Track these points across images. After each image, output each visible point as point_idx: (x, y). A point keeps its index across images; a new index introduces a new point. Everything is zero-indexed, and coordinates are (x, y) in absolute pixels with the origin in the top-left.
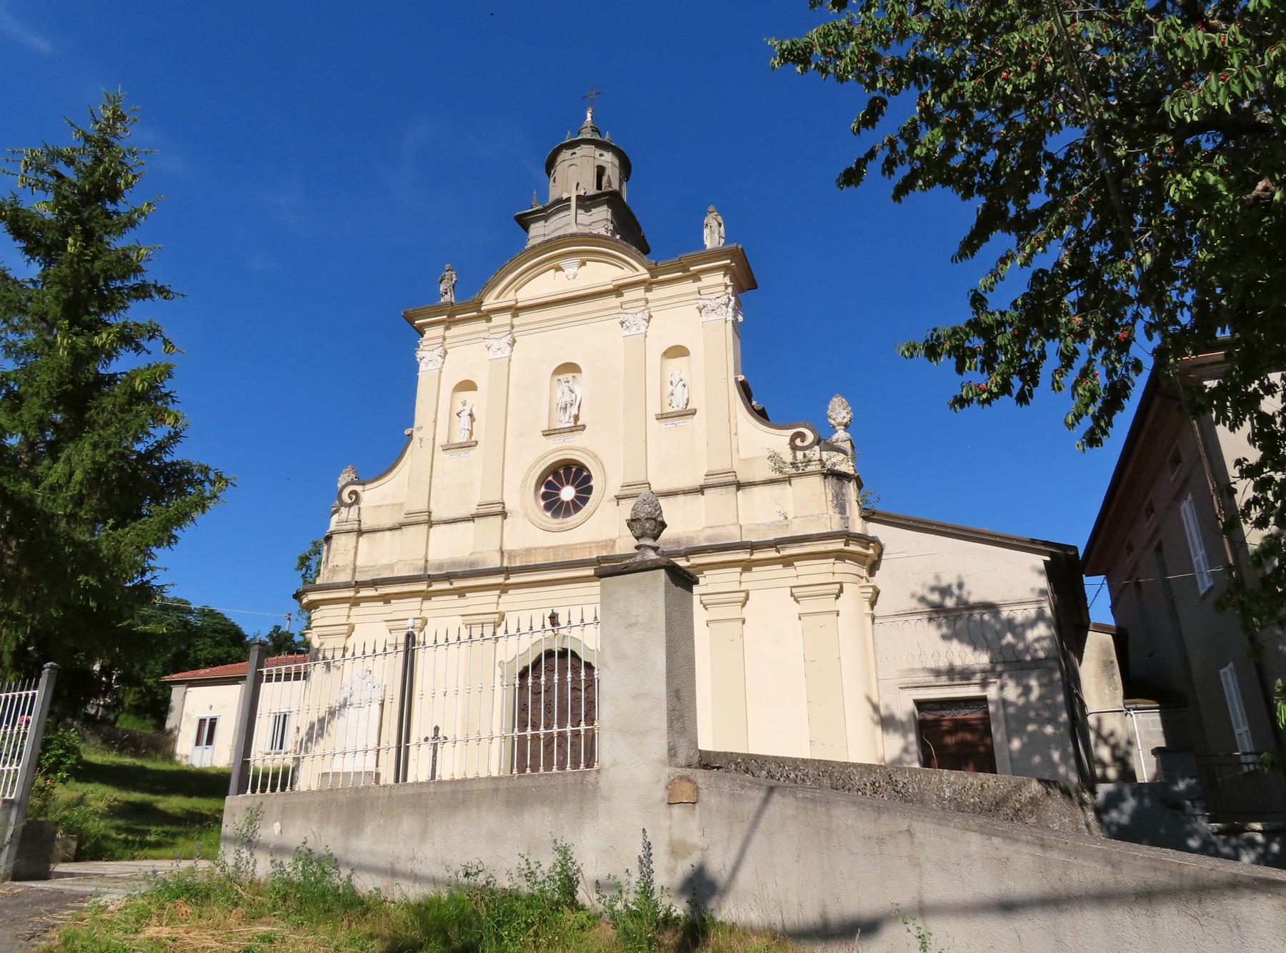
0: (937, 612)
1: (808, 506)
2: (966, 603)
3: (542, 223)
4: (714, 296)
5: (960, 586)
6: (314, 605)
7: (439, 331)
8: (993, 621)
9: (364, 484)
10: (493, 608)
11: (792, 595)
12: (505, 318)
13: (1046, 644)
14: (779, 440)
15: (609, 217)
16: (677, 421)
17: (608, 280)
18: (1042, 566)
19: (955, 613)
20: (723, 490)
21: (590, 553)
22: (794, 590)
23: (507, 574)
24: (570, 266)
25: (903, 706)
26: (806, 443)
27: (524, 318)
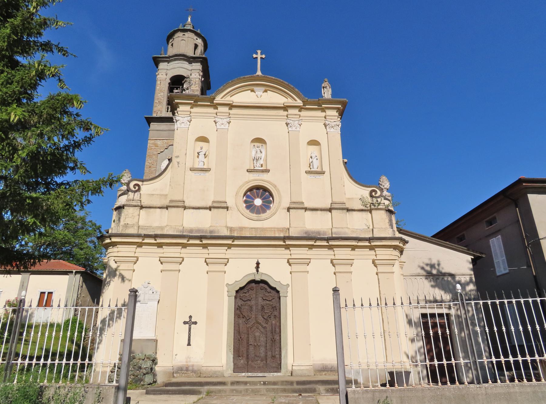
0: (429, 275)
1: (381, 224)
2: (441, 273)
3: (166, 63)
4: (333, 121)
5: (439, 265)
6: (107, 246)
7: (187, 108)
8: (452, 281)
9: (143, 181)
10: (178, 255)
11: (206, 261)
12: (226, 109)
13: (474, 292)
14: (365, 192)
15: (201, 69)
16: (316, 175)
17: (283, 102)
18: (470, 260)
19: (438, 277)
20: (341, 211)
21: (275, 233)
22: (161, 259)
23: (234, 240)
24: (259, 91)
25: (416, 315)
26: (377, 195)
27: (234, 111)
